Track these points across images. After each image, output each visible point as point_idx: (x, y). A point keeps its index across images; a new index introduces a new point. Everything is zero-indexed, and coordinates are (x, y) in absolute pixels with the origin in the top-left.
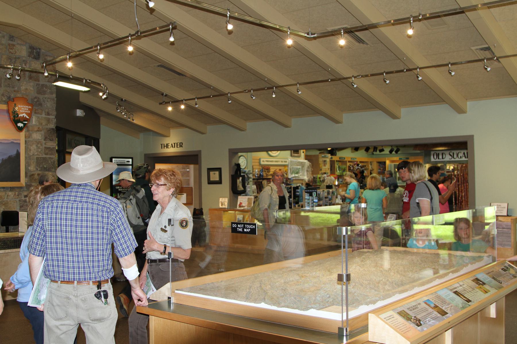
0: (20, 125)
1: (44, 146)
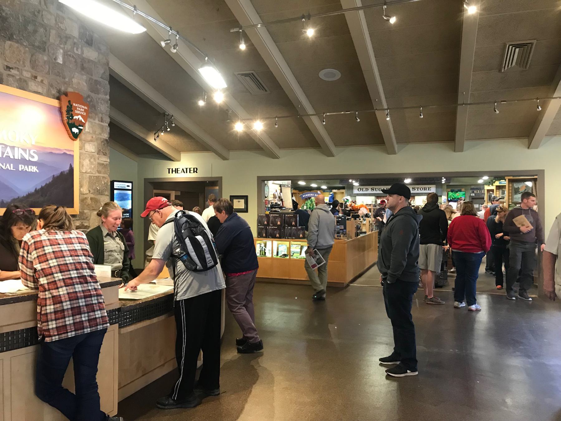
0: (75, 130)
1: (97, 161)
